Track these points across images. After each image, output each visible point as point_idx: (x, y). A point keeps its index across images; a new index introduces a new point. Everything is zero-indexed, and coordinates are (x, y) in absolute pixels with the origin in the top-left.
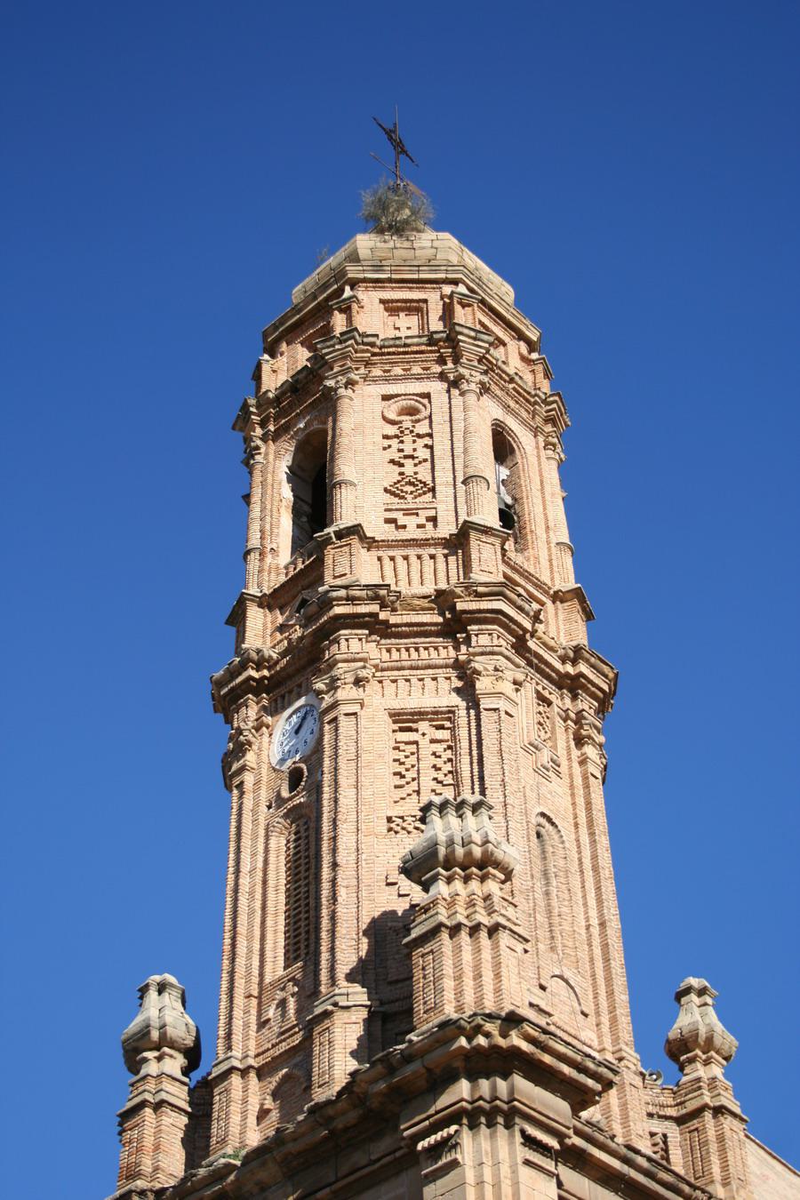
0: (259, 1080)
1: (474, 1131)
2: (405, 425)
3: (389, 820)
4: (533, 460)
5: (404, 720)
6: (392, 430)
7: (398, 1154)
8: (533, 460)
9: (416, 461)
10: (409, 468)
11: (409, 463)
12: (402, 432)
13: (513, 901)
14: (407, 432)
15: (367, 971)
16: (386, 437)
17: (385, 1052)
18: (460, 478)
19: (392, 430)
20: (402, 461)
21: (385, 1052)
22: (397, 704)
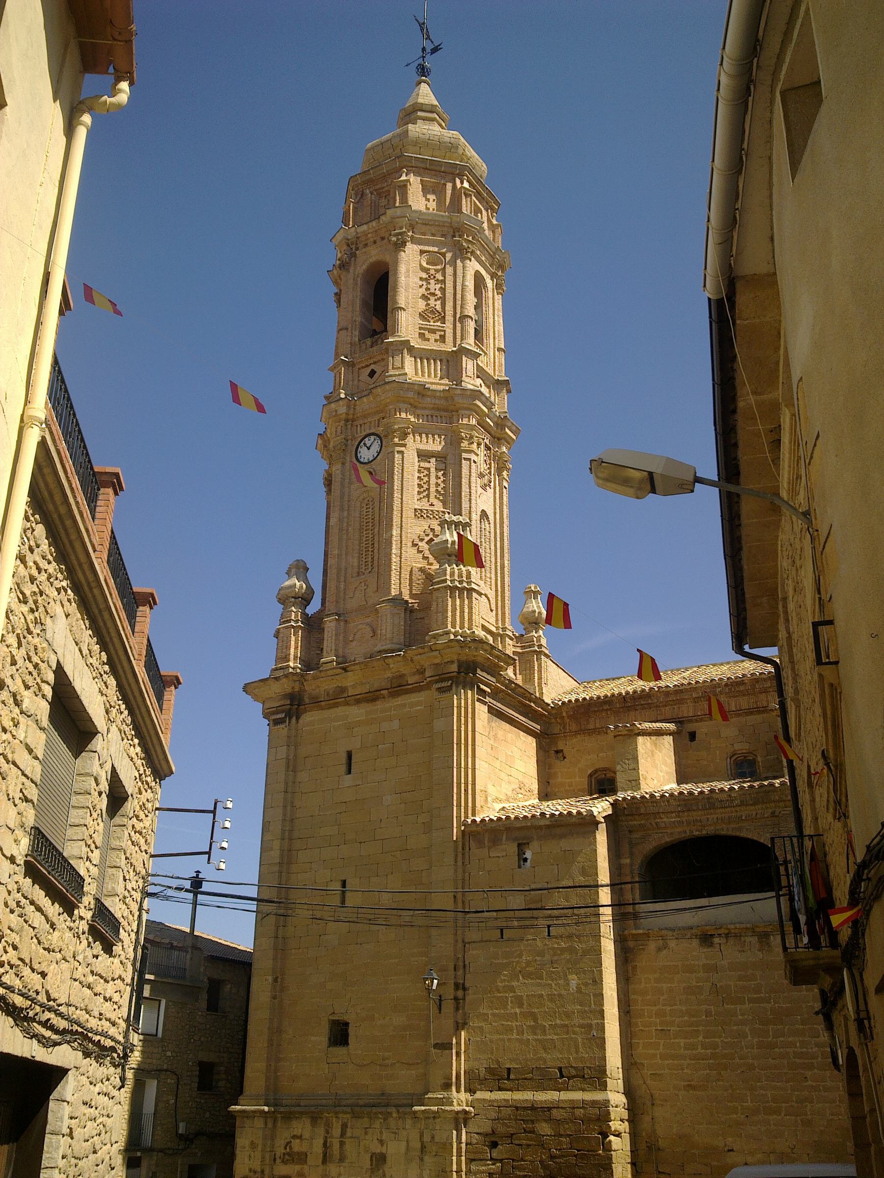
0: (199, 1088)
1: (609, 775)
2: (432, 272)
3: (415, 509)
4: (490, 294)
5: (423, 456)
6: (424, 276)
7: (421, 684)
8: (490, 294)
9: (436, 297)
10: (432, 302)
11: (432, 299)
12: (429, 277)
13: (24, 779)
14: (432, 277)
15: (33, 426)
16: (421, 279)
17: (708, 1028)
18: (458, 316)
19: (424, 276)
20: (429, 296)
21: (708, 1028)
22: (422, 447)
